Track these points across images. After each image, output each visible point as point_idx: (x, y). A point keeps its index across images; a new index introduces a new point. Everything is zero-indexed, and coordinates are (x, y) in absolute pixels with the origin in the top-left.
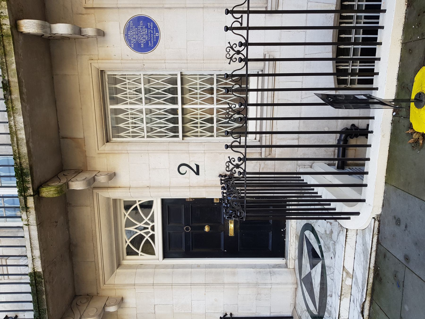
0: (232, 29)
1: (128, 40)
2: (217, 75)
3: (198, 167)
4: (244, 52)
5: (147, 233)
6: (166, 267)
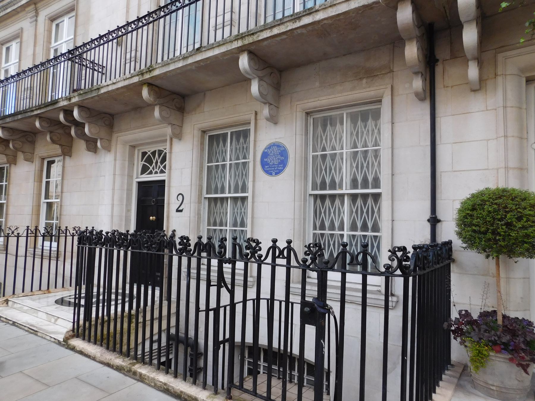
0: (28, 230)
1: (270, 147)
2: (246, 231)
3: (181, 211)
4: (13, 235)
6: (130, 185)
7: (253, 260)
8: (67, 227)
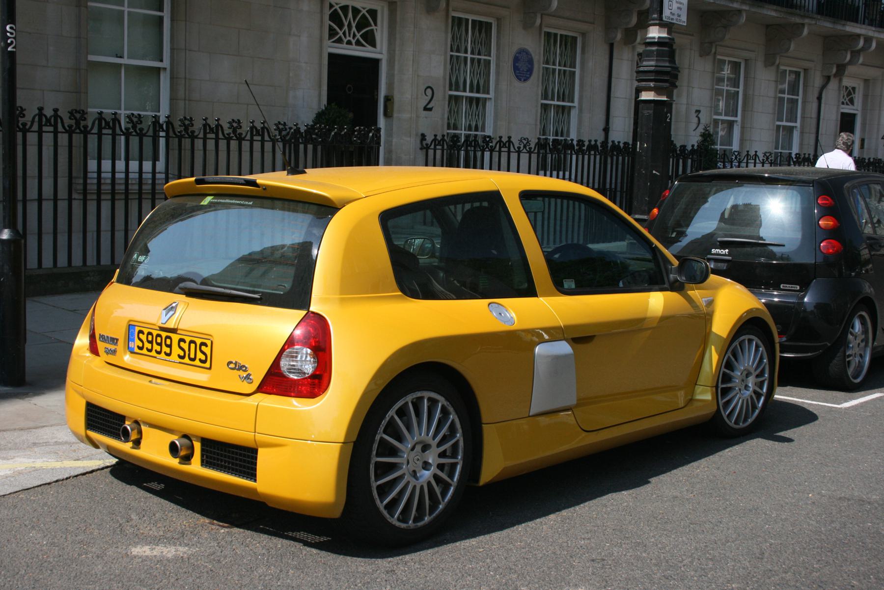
3: (430, 109)
5: (344, 33)
7: (487, 149)
8: (756, 152)
